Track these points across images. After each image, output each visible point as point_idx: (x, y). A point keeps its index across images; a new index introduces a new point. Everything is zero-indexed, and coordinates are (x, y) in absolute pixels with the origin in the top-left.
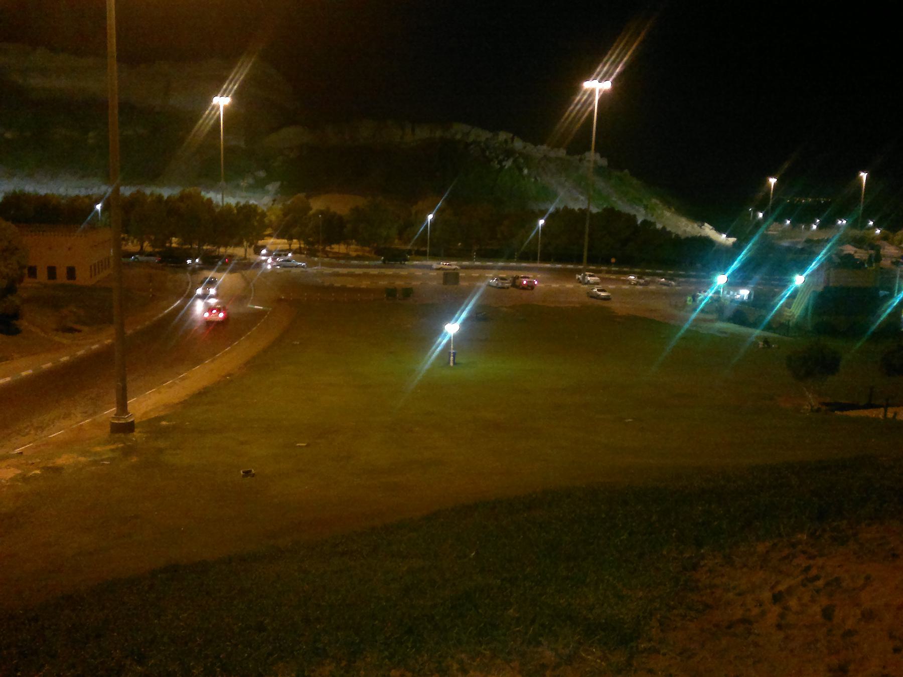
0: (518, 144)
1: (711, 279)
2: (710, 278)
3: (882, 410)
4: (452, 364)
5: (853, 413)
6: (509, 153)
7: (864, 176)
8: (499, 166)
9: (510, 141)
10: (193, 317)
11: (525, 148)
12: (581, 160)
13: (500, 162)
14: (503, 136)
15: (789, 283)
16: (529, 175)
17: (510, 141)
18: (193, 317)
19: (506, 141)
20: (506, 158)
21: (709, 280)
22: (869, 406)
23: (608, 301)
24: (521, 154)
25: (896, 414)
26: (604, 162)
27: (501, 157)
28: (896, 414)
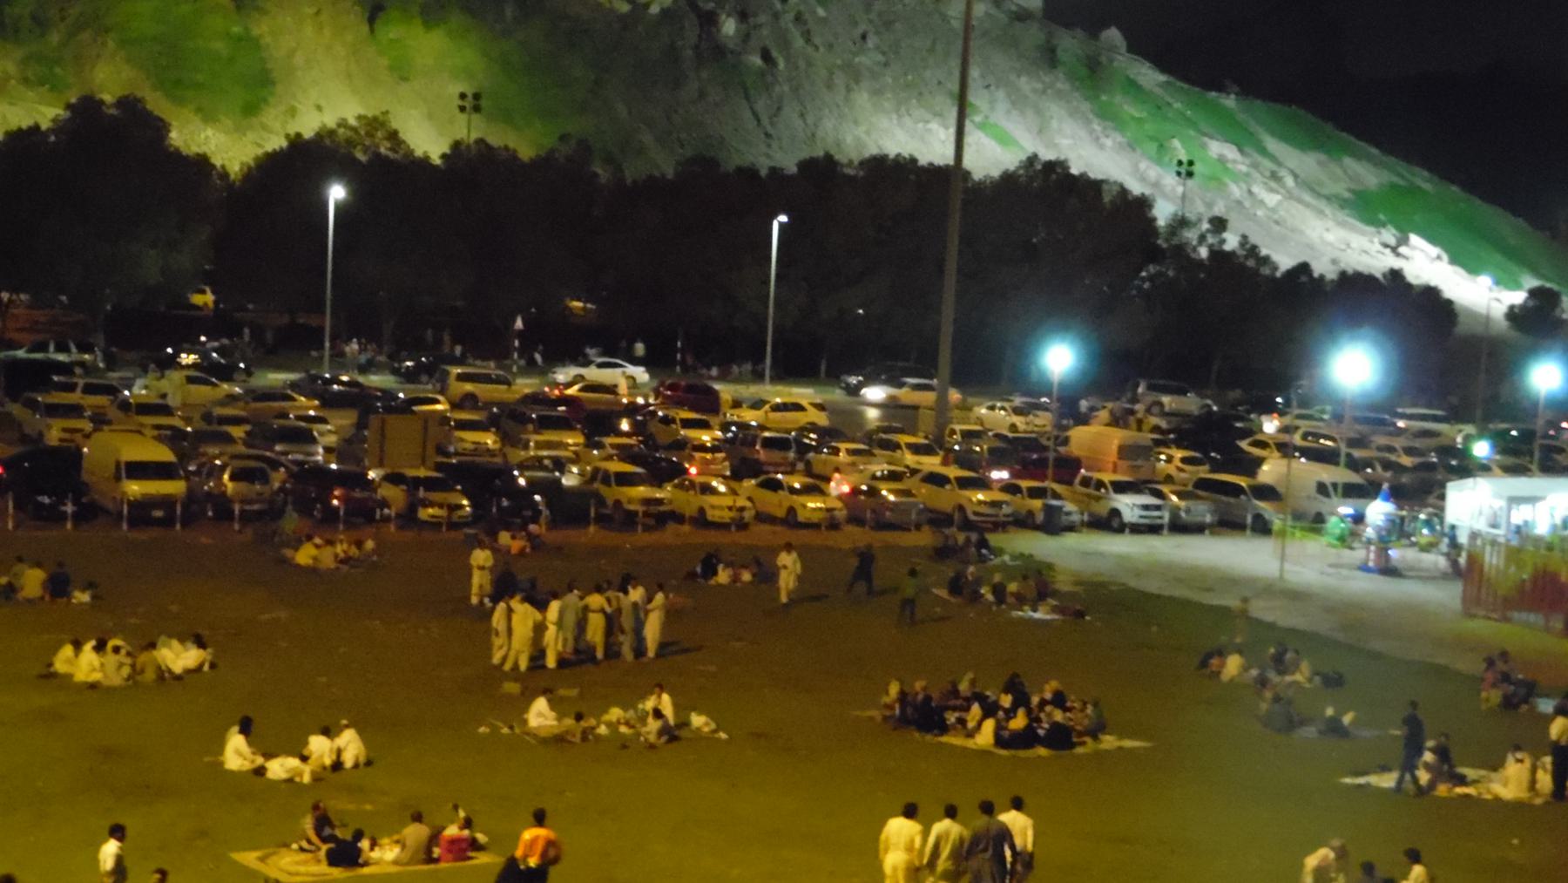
2: (1052, 384)
16: (746, 38)
18: (1542, 401)
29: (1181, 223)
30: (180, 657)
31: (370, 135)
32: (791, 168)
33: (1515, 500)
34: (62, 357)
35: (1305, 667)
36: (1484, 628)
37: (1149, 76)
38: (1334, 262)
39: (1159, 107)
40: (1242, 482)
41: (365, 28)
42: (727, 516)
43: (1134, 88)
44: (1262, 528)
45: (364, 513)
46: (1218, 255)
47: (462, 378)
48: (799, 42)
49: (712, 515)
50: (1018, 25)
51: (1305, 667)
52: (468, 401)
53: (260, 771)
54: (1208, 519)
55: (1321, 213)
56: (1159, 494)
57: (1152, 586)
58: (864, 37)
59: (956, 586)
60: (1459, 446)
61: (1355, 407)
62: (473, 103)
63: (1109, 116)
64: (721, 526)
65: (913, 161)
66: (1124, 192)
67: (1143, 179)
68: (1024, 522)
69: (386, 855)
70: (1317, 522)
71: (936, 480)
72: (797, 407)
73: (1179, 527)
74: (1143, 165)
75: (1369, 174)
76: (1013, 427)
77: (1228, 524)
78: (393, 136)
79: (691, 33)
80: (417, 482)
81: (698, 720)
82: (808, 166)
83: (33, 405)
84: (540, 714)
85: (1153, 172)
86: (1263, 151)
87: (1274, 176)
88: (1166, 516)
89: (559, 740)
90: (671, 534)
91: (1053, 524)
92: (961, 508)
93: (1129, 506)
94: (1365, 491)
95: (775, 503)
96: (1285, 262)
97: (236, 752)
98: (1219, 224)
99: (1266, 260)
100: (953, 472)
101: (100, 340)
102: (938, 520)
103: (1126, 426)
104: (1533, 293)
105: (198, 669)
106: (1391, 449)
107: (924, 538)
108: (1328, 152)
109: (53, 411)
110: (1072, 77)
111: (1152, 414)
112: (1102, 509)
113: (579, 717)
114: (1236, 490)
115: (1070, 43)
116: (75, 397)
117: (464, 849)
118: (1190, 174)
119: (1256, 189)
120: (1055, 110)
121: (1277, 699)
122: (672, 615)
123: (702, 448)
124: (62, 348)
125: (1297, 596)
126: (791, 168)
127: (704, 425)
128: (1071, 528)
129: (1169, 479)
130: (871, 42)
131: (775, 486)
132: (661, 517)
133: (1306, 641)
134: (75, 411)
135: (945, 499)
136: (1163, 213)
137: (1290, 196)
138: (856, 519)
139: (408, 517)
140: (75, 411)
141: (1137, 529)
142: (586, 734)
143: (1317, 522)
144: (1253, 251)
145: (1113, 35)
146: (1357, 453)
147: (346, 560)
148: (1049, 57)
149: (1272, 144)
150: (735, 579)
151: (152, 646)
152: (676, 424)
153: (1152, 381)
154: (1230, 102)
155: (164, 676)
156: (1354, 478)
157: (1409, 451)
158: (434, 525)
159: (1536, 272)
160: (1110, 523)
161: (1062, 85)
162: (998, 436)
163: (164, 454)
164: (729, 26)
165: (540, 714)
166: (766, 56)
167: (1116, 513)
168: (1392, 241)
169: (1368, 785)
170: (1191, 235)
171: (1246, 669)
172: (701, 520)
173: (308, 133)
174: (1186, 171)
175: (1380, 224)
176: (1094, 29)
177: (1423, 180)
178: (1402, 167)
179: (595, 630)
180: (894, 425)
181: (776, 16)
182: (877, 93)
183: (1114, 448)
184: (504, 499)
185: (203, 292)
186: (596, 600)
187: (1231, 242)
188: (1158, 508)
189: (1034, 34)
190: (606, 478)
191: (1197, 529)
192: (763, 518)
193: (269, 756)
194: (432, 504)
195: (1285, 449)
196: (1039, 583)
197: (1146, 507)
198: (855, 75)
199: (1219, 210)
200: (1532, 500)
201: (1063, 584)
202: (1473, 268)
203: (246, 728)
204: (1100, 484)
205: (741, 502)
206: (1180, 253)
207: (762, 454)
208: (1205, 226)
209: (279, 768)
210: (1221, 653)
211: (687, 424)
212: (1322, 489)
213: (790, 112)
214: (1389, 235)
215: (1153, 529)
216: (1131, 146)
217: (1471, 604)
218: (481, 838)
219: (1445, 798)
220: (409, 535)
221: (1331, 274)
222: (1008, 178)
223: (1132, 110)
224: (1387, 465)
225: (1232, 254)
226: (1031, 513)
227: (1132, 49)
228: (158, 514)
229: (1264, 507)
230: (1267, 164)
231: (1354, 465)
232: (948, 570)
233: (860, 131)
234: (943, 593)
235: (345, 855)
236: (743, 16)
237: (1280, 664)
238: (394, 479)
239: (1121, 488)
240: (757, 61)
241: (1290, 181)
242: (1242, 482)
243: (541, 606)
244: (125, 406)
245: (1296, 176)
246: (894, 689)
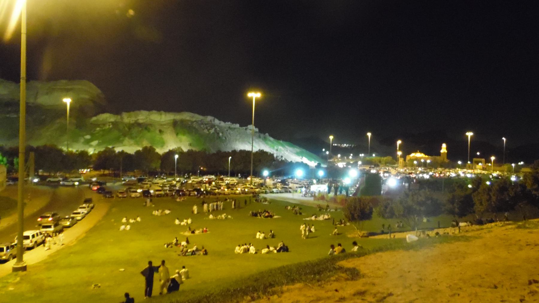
0: (217, 122)
1: (291, 283)
2: (270, 173)
3: (389, 235)
4: (233, 207)
5: (377, 237)
6: (213, 126)
7: (369, 134)
8: (208, 132)
9: (212, 121)
10: (321, 177)
11: (220, 123)
12: (246, 129)
13: (208, 130)
14: (209, 118)
15: (475, 179)
16: (223, 136)
17: (212, 121)
18: (321, 177)
19: (211, 121)
20: (211, 129)
21: (271, 172)
22: (383, 233)
23: (32, 251)
24: (218, 126)
25: (394, 236)
26: (257, 130)
27: (209, 128)
28: (394, 236)
29: (277, 157)
30: (167, 212)
31: (179, 149)
32: (230, 151)
33: (318, 187)
34: (144, 178)
35: (298, 207)
36: (317, 202)
37: (271, 139)
38: (295, 160)
39: (273, 143)
40: (287, 187)
41: (176, 136)
42: (227, 194)
43: (270, 141)
44: (290, 192)
45: (184, 195)
46: (282, 160)
47: (193, 178)
48: (229, 136)
49: (225, 193)
50: (256, 133)
51: (298, 207)
52: (193, 181)
53: (180, 224)
54: (284, 191)
55: (293, 155)
56: (278, 189)
57: (278, 199)
58: (237, 135)
59: (256, 200)
60: (537, 185)
61: (529, 168)
62: (190, 145)
63: (267, 144)
64: (226, 195)
65: (245, 150)
66: (270, 153)
67: (272, 151)
68: (263, 193)
69: (197, 232)
70: (296, 191)
71: (252, 188)
72: (233, 180)
73: (280, 192)
74: (271, 149)
75: (298, 150)
76: (259, 182)
77: (286, 192)
78: (181, 149)
79: (216, 135)
80: (190, 191)
81: (229, 217)
82: (233, 151)
83: (142, 183)
84: (211, 216)
85: (273, 150)
86: (286, 148)
87: (287, 151)
88: (279, 192)
89: (214, 220)
90: (221, 196)
91: (266, 193)
92: (255, 192)
93: (275, 190)
94: (302, 187)
95: (233, 192)
96: (289, 161)
97: (177, 222)
98: (282, 157)
99: (288, 161)
100: (254, 187)
101: (147, 175)
102: (253, 193)
103: (532, 293)
104: (318, 164)
105: (169, 213)
106: (303, 182)
107: (251, 195)
108: (293, 147)
109: (145, 184)
110: (262, 139)
111: (366, 175)
112: (272, 191)
113: (216, 217)
114: (287, 188)
115: (262, 135)
116: (147, 182)
117: (206, 231)
118: (277, 151)
119: (285, 152)
120: (261, 143)
121: (295, 211)
122: (224, 205)
123: (223, 185)
124: (144, 176)
125: (295, 200)
126: (230, 151)
127: (223, 183)
128: (268, 193)
129: (278, 187)
130: (238, 136)
131: (233, 190)
132: (220, 194)
133: (298, 205)
134: (147, 184)
135: (253, 190)
136: (275, 156)
137: (289, 153)
138: (243, 193)
139: (189, 195)
140: (147, 184)
141: (276, 193)
142: (217, 219)
143: (296, 191)
144: (286, 160)
145: (267, 134)
146: (300, 183)
147: (183, 200)
148: (260, 137)
149: (287, 147)
150: (230, 201)
151: (164, 211)
152: (491, 163)
153: (398, 149)
154: (281, 142)
155: (166, 214)
156: (300, 186)
157: (306, 183)
158: (192, 196)
159: (318, 161)
160: (272, 192)
161: (261, 140)
162: (258, 183)
163: (160, 188)
164: (221, 134)
165: (211, 216)
166: (225, 138)
167: (273, 191)
168: (301, 158)
169: (306, 220)
170: (278, 158)
171: (291, 208)
172: (224, 194)
173: (171, 149)
174: (277, 150)
175: (299, 156)
176: (265, 134)
177: (304, 150)
178: (302, 149)
179: (215, 207)
180: (504, 157)
181: (226, 133)
182: (239, 142)
183: (173, 277)
184: (352, 155)
185: (331, 178)
186: (215, 204)
187: (283, 159)
188: (278, 190)
189: (258, 134)
190: (213, 190)
191: (283, 193)
192: (232, 193)
193: (181, 222)
194: (192, 193)
195: (292, 183)
196: (265, 199)
197: (277, 190)
198: (236, 140)
199: (281, 155)
200: (320, 187)
201: (268, 199)
202: (311, 161)
203: (178, 219)
204: (271, 188)
205: (229, 192)
206: (278, 160)
207: (230, 186)
208: (280, 157)
209: (182, 224)
210: (288, 206)
211: (221, 183)
212: (297, 187)
213: (229, 145)
214: (301, 157)
215: (277, 193)
216: (270, 147)
217: (314, 200)
218: (208, 230)
219: (217, 118)
220: (190, 197)
221: (295, 162)
222: (257, 152)
223: (269, 143)
224: (303, 184)
225: (283, 160)
226: (263, 192)
227: (269, 136)
228: (160, 196)
229: (290, 190)
230: (286, 149)
231: (300, 184)
232: (255, 199)
233: (237, 146)
234: (254, 201)
235: (193, 232)
236: (222, 133)
237: (294, 207)
238: (188, 190)
239: (273, 188)
240: (224, 138)
241: (289, 151)
242: (287, 187)
243: (208, 204)
244: (153, 183)
245: (290, 151)
246: (251, 212)
